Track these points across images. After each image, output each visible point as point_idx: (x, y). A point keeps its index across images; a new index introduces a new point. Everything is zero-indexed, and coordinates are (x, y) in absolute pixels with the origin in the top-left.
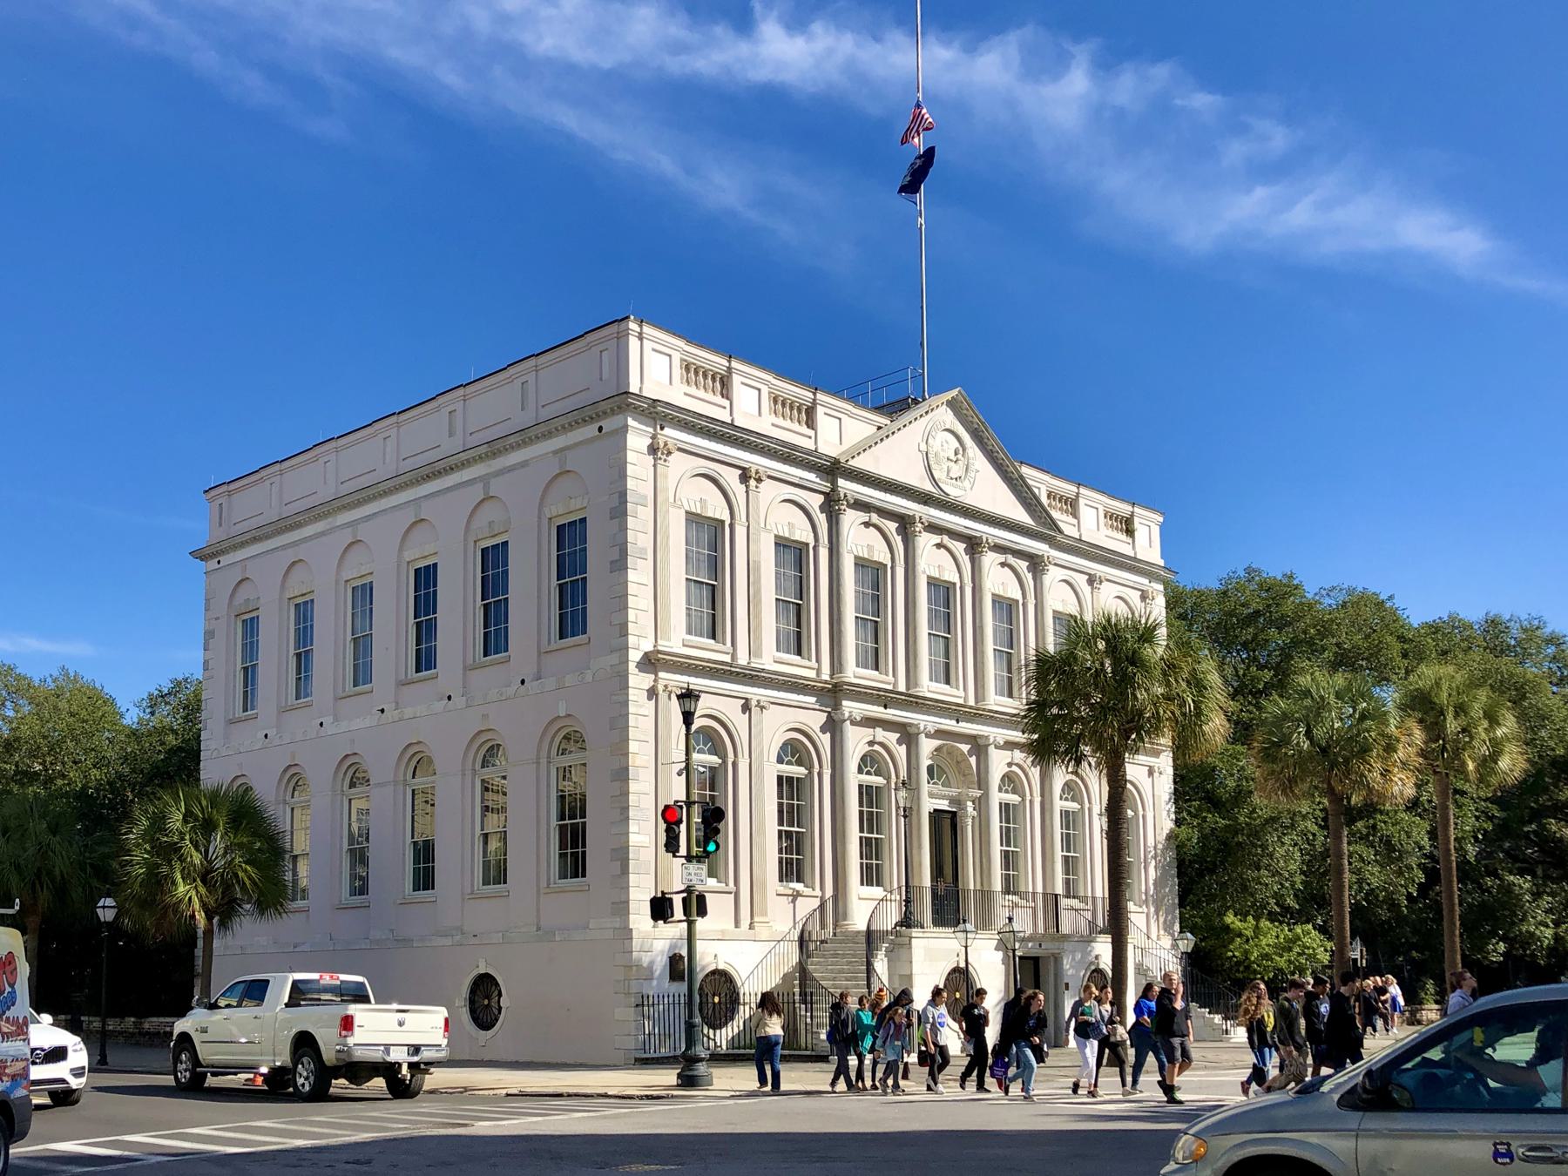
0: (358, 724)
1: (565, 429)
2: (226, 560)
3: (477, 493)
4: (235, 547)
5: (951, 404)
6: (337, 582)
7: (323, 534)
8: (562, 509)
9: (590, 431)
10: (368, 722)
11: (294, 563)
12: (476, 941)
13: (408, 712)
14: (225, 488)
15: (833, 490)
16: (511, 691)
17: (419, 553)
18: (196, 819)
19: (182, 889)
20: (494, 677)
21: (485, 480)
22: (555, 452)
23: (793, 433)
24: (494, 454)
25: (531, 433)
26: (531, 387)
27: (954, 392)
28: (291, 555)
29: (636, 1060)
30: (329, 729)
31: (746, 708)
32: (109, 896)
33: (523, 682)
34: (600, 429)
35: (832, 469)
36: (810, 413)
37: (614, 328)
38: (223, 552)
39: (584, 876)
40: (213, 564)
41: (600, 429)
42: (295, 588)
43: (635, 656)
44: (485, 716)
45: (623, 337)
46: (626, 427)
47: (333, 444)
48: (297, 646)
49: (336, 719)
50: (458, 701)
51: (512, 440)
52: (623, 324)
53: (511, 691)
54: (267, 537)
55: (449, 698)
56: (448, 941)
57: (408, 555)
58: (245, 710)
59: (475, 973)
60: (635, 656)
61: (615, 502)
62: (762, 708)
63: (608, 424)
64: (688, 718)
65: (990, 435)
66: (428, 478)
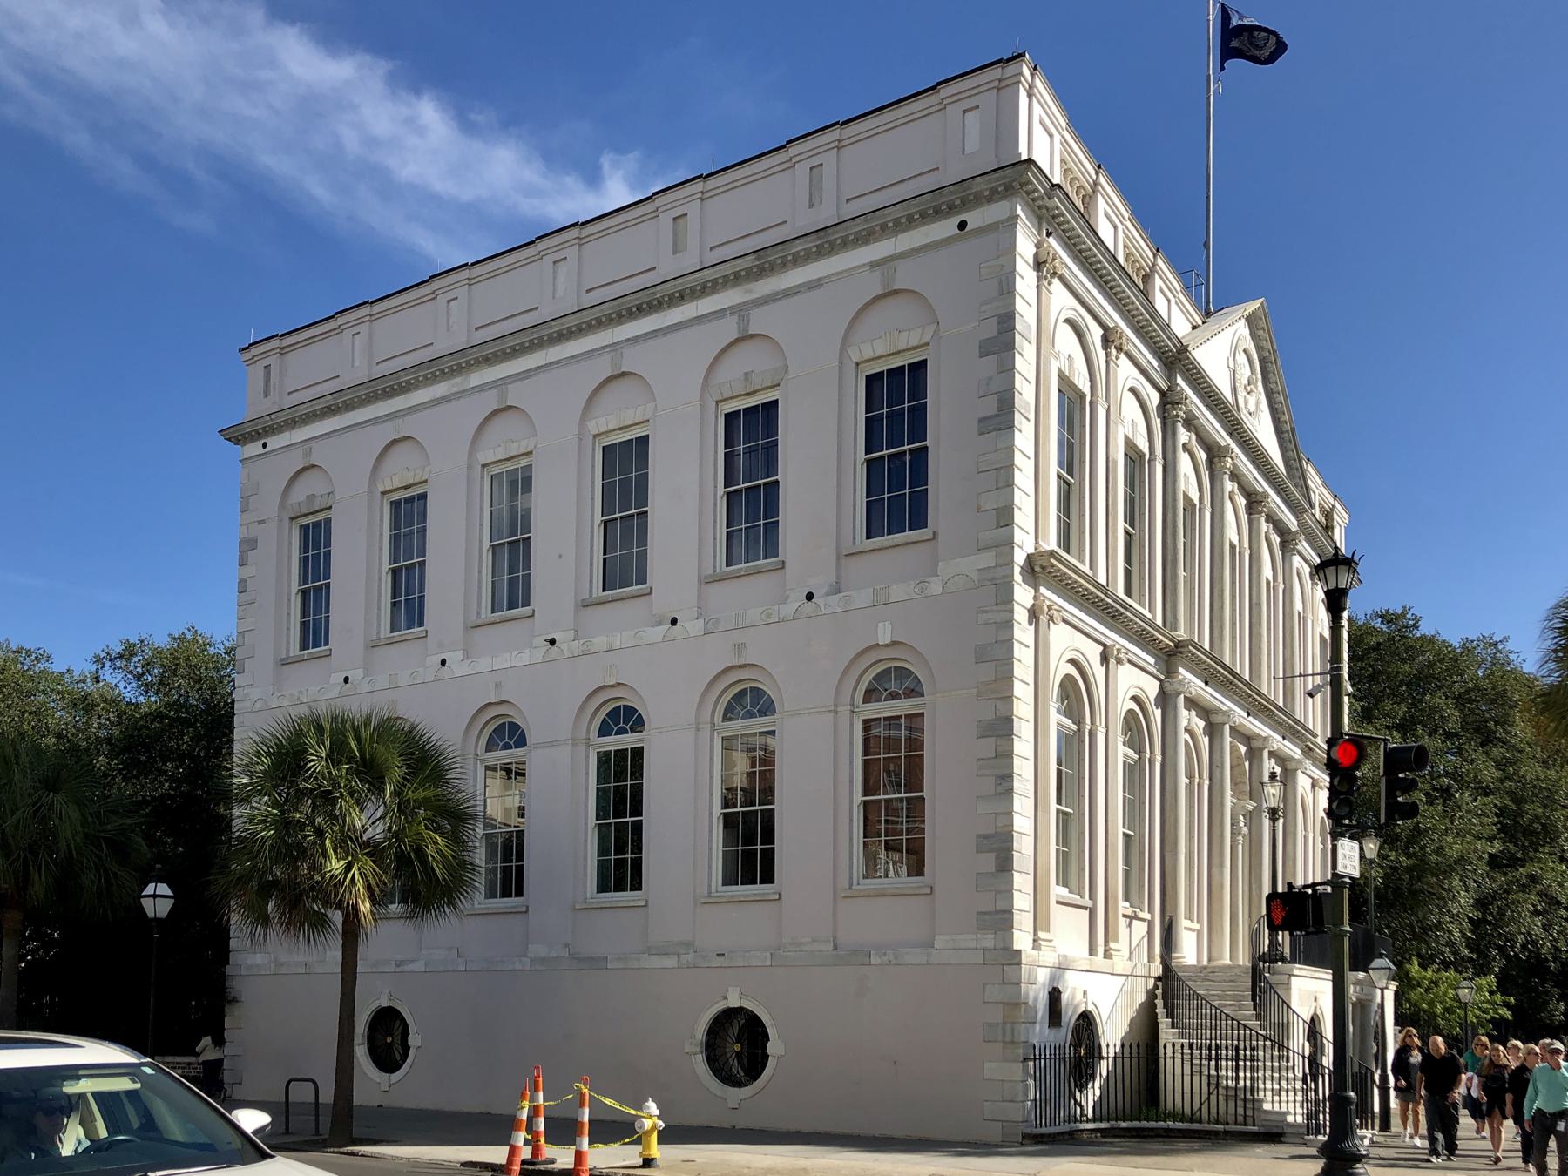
0: (507, 660)
1: (898, 227)
2: (274, 442)
3: (728, 329)
4: (293, 423)
5: (1250, 320)
6: (470, 467)
7: (445, 399)
8: (884, 346)
9: (948, 227)
10: (525, 658)
11: (394, 442)
12: (720, 961)
13: (599, 642)
14: (276, 343)
15: (1170, 388)
16: (788, 610)
17: (616, 418)
18: (351, 759)
19: (335, 865)
20: (751, 594)
21: (741, 310)
22: (874, 265)
24: (760, 272)
25: (837, 235)
26: (829, 172)
27: (1254, 306)
28: (390, 432)
29: (1025, 1136)
30: (458, 666)
31: (1105, 658)
32: (159, 880)
33: (810, 597)
34: (962, 225)
37: (995, 73)
38: (274, 430)
39: (519, 893)
40: (254, 448)
41: (962, 225)
42: (400, 473)
43: (1020, 558)
44: (740, 647)
45: (1007, 88)
46: (1014, 218)
47: (465, 274)
48: (395, 558)
49: (467, 656)
50: (691, 626)
51: (799, 247)
52: (1011, 69)
53: (788, 610)
54: (349, 406)
55: (674, 622)
56: (670, 962)
57: (593, 427)
58: (304, 646)
59: (720, 1006)
60: (1020, 558)
61: (991, 329)
63: (975, 218)
64: (1335, 600)
65: (1277, 366)
66: (640, 311)
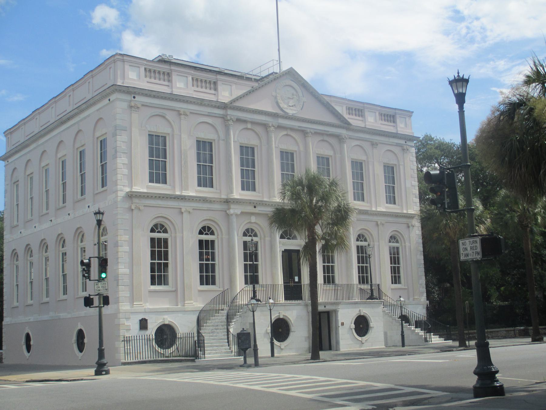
23: (207, 95)
35: (225, 106)
36: (215, 83)
62: (383, 224)
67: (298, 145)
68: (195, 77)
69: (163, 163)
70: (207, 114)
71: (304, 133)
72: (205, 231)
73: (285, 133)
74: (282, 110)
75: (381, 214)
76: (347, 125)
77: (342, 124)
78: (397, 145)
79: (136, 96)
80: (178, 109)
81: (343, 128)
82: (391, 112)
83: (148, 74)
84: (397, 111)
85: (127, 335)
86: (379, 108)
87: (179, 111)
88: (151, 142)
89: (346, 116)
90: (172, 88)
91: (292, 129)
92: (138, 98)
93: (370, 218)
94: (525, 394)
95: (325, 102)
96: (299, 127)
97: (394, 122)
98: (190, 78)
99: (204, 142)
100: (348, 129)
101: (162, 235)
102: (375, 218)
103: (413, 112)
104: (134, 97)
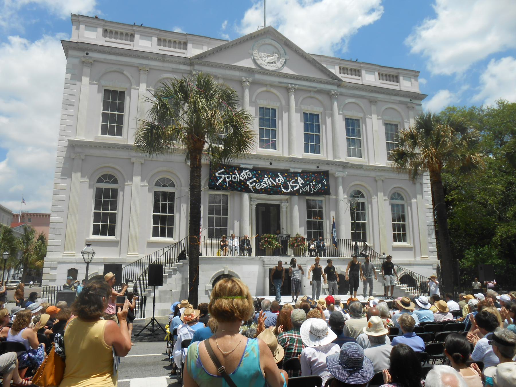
67: (280, 101)
68: (342, 66)
69: (359, 141)
70: (171, 70)
71: (288, 90)
72: (106, 179)
73: (264, 89)
74: (259, 66)
75: (382, 170)
76: (338, 82)
77: (331, 80)
78: (401, 103)
79: (89, 53)
80: (136, 65)
81: (333, 84)
82: (393, 72)
83: (381, 77)
84: (400, 71)
85: (51, 285)
86: (378, 68)
87: (138, 67)
88: (347, 124)
89: (340, 76)
90: (400, 87)
91: (272, 86)
92: (91, 54)
93: (367, 173)
94: (436, 356)
95: (311, 60)
96: (105, 59)
97: (398, 82)
98: (377, 74)
99: (311, 115)
100: (339, 86)
101: (400, 202)
102: (373, 174)
103: (419, 72)
104: (87, 54)
